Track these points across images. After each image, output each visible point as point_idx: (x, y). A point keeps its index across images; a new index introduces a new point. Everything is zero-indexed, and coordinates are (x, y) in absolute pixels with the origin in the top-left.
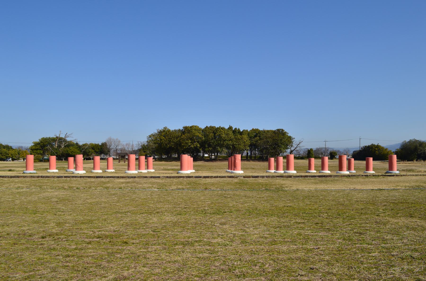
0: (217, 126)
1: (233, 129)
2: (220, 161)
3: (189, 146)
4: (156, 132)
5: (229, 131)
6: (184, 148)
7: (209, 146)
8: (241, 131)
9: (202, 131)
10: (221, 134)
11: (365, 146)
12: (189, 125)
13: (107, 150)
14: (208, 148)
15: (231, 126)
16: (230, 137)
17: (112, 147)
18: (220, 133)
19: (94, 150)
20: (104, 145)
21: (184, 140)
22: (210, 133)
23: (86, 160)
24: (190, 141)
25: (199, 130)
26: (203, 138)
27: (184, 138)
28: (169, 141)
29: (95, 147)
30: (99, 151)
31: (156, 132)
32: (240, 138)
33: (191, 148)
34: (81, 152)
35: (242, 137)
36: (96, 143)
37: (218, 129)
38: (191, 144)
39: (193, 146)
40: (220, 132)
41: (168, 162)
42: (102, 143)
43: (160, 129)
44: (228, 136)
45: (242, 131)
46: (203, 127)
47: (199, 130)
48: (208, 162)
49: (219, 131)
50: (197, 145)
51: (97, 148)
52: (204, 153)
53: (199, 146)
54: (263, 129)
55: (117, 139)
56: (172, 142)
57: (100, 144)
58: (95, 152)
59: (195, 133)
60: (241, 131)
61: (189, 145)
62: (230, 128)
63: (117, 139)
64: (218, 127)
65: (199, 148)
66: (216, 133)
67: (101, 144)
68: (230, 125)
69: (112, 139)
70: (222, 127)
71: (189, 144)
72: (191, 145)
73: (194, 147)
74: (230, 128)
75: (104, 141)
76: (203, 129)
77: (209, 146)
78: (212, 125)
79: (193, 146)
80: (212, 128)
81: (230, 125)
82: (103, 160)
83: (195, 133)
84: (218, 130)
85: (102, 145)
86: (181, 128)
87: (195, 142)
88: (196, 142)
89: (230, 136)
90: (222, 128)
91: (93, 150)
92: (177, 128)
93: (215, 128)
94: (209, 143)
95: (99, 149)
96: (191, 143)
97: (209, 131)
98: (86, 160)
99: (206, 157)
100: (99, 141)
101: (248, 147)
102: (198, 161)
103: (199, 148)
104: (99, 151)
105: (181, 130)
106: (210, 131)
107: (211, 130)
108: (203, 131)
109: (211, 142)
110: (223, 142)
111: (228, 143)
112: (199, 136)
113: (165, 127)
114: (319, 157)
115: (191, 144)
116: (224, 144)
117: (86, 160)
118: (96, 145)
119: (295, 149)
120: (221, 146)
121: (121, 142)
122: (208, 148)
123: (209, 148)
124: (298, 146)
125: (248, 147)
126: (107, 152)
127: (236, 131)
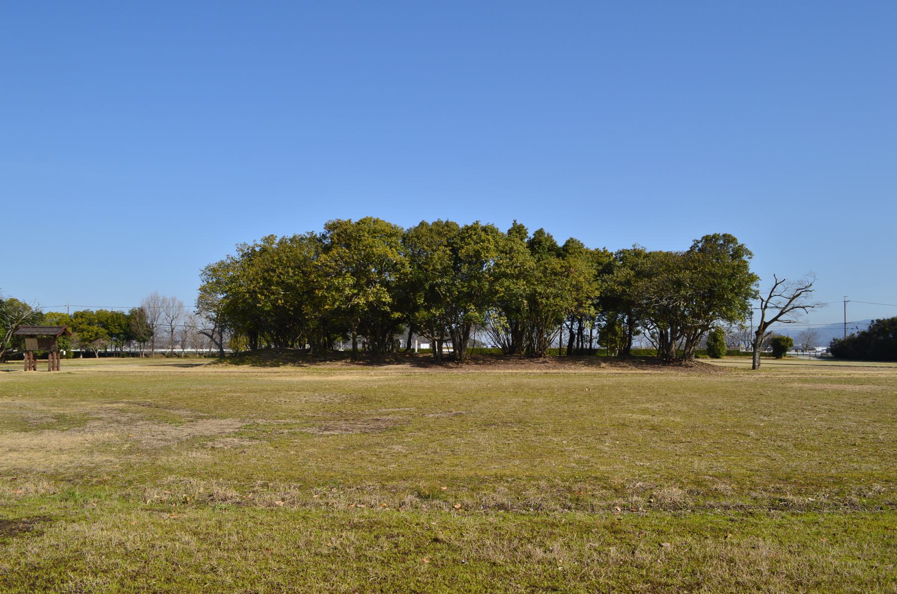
0: (463, 221)
1: (531, 235)
2: (477, 364)
3: (349, 299)
4: (237, 256)
5: (514, 241)
6: (327, 307)
7: (434, 298)
8: (561, 243)
9: (404, 239)
10: (483, 248)
11: (878, 321)
12: (352, 215)
13: (145, 328)
14: (428, 308)
15: (518, 223)
16: (522, 264)
17: (159, 321)
18: (477, 247)
19: (108, 329)
20: (139, 315)
21: (327, 275)
22: (434, 248)
23: (83, 357)
24: (351, 281)
25: (391, 235)
26: (407, 265)
27: (327, 266)
28: (264, 279)
29: (109, 321)
30: (122, 331)
31: (237, 256)
32: (559, 270)
33: (353, 306)
34: (8, 329)
35: (567, 264)
36: (115, 310)
37: (467, 233)
38: (356, 291)
39: (362, 301)
40: (476, 243)
41: (265, 366)
42: (131, 309)
43: (251, 244)
44: (511, 259)
45: (566, 245)
46: (406, 222)
47: (391, 235)
48: (427, 370)
49: (475, 237)
50: (380, 297)
51: (116, 324)
52: (414, 335)
53: (387, 299)
54: (634, 246)
55: (174, 300)
56: (277, 282)
57: (127, 313)
58: (108, 334)
59: (371, 247)
60: (561, 243)
61: (347, 297)
62: (518, 230)
63: (174, 300)
64: (470, 224)
65: (388, 309)
66: (463, 248)
67: (130, 312)
68: (515, 221)
69: (161, 298)
70: (483, 224)
71: (347, 291)
72: (354, 295)
73: (369, 304)
74: (518, 230)
75: (137, 305)
76: (405, 230)
77: (434, 298)
78: (442, 220)
79: (362, 301)
80: (443, 229)
81: (515, 221)
82: (133, 357)
83: (371, 247)
84: (470, 236)
85: (132, 315)
86: (319, 230)
87: (370, 283)
88: (378, 286)
89: (521, 260)
90: (484, 229)
91: (103, 330)
92: (302, 231)
93: (454, 227)
94: (432, 287)
95: (120, 325)
96: (354, 286)
97: (432, 237)
98: (81, 356)
99: (638, 351)
100: (123, 305)
101: (593, 304)
102: (389, 363)
103: (388, 309)
104: (122, 331)
105: (318, 236)
106: (437, 238)
107: (439, 234)
108: (405, 238)
109: (439, 285)
110: (492, 283)
111: (512, 287)
112: (390, 256)
113: (267, 236)
114: (738, 351)
115: (356, 291)
116: (497, 292)
117: (81, 356)
118: (115, 316)
119: (781, 314)
120: (483, 301)
121: (186, 309)
122: (428, 308)
123: (433, 311)
124: (795, 302)
125: (592, 308)
126: (145, 334)
127: (540, 243)
